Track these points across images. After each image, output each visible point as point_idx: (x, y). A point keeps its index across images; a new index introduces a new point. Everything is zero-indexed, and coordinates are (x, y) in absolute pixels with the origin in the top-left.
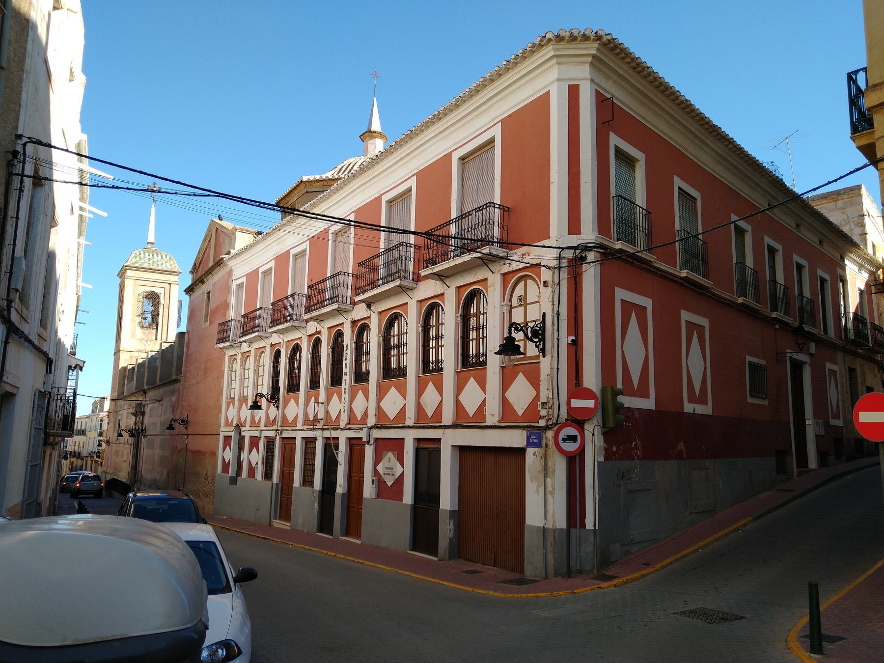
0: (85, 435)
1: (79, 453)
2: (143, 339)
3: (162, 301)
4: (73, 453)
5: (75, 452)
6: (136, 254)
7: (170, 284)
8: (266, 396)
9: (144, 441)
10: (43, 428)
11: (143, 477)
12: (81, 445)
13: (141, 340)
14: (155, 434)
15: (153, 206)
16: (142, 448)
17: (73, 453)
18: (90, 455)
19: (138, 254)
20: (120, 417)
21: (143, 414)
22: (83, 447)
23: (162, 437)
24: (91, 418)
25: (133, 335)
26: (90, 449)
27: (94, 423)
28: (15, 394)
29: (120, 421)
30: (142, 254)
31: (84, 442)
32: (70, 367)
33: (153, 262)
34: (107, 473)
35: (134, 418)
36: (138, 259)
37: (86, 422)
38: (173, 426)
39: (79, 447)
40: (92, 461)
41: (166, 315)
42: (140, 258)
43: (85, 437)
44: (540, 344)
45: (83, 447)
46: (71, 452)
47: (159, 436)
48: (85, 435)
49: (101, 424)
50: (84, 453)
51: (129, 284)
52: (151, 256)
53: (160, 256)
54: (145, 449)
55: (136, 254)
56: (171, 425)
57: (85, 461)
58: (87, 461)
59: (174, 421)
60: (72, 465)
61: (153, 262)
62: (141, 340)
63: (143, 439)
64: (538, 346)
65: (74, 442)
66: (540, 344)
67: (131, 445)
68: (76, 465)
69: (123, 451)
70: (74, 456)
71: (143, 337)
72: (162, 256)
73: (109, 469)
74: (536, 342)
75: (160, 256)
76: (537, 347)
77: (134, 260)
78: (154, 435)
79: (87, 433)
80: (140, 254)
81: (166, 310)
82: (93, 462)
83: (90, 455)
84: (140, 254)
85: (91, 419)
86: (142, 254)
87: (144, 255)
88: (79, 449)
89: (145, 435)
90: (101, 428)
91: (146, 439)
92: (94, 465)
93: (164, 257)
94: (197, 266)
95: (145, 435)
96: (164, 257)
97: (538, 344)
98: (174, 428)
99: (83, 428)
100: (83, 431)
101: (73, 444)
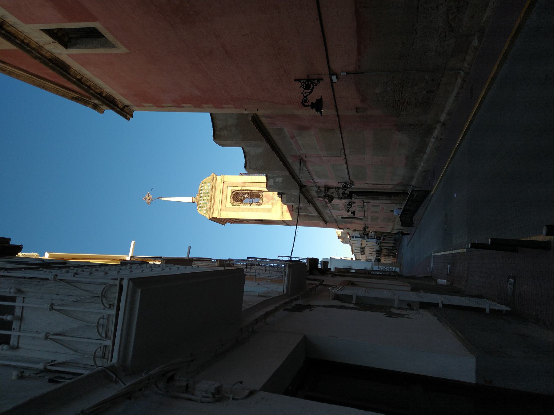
0: (364, 248)
1: (377, 251)
2: (272, 203)
3: (240, 188)
4: (378, 255)
5: (377, 254)
6: (200, 211)
7: (224, 183)
8: (305, 95)
9: (359, 185)
10: (403, 208)
11: (401, 183)
12: (371, 250)
13: (272, 204)
14: (345, 165)
15: (162, 199)
16: (366, 186)
17: (378, 255)
18: (378, 244)
19: (200, 209)
20: (340, 218)
21: (327, 188)
22: (373, 248)
23: (347, 152)
24: (352, 244)
25: (269, 210)
26: (374, 244)
27: (356, 242)
28: (305, 337)
29: (343, 218)
30: (200, 205)
31: (369, 248)
32: (24, 298)
33: (206, 196)
34: (393, 228)
35: (335, 201)
36: (204, 209)
37: (355, 247)
38: (314, 102)
39: (373, 251)
40: (383, 243)
41: (251, 185)
42: (203, 207)
43: (366, 248)
44: (315, 83)
45: (373, 248)
46: (377, 256)
47: (347, 157)
48: (364, 248)
49: (356, 237)
50: (377, 248)
51: (224, 215)
52: (201, 198)
53: (202, 192)
54: (366, 182)
55: (200, 211)
56: (313, 106)
57: (383, 247)
58: (383, 246)
59: (306, 101)
60: (386, 255)
61: (206, 196)
62: (272, 204)
63: (357, 186)
64: (316, 84)
65: (370, 254)
66: (315, 83)
67: (364, 202)
68: (386, 253)
69: (372, 212)
70: (380, 254)
71: (270, 202)
72: (201, 190)
73: (390, 227)
74: (313, 86)
75: (202, 192)
76: (316, 85)
77: (205, 212)
78: (348, 169)
79: (363, 246)
80: (200, 207)
81: (247, 185)
82: (384, 241)
83: (378, 244)
84: (200, 207)
85: (353, 244)
86: (200, 205)
87: (201, 204)
88: (375, 251)
89: (350, 183)
90: (359, 237)
91: (355, 182)
92: (386, 241)
93: (202, 188)
94: (76, 95)
95: (350, 183)
96: (202, 188)
97: (315, 85)
98: (317, 100)
99: (360, 249)
100: (361, 249)
101: (371, 255)
